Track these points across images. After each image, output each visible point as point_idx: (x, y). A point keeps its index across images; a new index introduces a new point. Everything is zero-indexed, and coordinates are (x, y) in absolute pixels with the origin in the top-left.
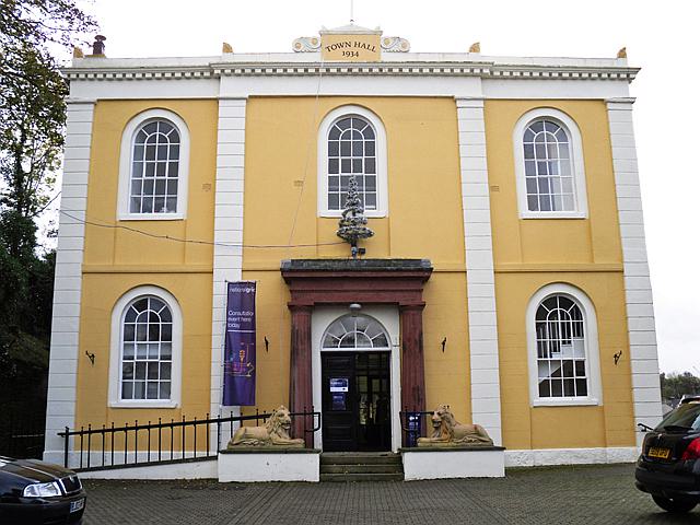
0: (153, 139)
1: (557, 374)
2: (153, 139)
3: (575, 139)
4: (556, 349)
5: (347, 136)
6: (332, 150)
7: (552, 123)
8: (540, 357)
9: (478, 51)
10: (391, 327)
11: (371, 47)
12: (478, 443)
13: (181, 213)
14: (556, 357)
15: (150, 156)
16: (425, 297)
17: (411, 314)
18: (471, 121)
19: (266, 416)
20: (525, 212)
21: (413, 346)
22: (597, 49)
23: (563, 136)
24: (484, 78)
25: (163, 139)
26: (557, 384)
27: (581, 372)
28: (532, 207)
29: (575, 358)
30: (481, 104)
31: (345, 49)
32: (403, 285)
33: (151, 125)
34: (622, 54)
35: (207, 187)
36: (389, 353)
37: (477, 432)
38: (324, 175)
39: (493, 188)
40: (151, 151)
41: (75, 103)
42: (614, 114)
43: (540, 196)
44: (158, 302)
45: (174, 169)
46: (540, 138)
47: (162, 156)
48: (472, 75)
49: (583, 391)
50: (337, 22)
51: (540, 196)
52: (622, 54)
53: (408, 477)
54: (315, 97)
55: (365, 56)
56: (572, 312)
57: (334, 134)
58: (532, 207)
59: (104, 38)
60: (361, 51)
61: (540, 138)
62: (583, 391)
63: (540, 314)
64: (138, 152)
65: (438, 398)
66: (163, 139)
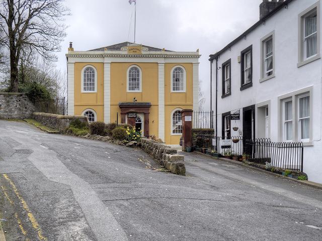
0: (88, 72)
1: (177, 128)
2: (133, 72)
3: (185, 73)
5: (88, 72)
7: (180, 69)
17: (146, 115)
18: (161, 69)
19: (320, 58)
20: (172, 91)
22: (192, 49)
23: (182, 72)
24: (165, 58)
28: (174, 90)
30: (164, 65)
32: (145, 108)
34: (198, 51)
35: (102, 85)
37: (160, 140)
39: (165, 85)
44: (91, 113)
45: (93, 81)
48: (162, 57)
52: (198, 51)
55: (138, 53)
58: (174, 90)
60: (137, 51)
63: (174, 115)
64: (85, 75)
65: (151, 134)
66: (90, 72)
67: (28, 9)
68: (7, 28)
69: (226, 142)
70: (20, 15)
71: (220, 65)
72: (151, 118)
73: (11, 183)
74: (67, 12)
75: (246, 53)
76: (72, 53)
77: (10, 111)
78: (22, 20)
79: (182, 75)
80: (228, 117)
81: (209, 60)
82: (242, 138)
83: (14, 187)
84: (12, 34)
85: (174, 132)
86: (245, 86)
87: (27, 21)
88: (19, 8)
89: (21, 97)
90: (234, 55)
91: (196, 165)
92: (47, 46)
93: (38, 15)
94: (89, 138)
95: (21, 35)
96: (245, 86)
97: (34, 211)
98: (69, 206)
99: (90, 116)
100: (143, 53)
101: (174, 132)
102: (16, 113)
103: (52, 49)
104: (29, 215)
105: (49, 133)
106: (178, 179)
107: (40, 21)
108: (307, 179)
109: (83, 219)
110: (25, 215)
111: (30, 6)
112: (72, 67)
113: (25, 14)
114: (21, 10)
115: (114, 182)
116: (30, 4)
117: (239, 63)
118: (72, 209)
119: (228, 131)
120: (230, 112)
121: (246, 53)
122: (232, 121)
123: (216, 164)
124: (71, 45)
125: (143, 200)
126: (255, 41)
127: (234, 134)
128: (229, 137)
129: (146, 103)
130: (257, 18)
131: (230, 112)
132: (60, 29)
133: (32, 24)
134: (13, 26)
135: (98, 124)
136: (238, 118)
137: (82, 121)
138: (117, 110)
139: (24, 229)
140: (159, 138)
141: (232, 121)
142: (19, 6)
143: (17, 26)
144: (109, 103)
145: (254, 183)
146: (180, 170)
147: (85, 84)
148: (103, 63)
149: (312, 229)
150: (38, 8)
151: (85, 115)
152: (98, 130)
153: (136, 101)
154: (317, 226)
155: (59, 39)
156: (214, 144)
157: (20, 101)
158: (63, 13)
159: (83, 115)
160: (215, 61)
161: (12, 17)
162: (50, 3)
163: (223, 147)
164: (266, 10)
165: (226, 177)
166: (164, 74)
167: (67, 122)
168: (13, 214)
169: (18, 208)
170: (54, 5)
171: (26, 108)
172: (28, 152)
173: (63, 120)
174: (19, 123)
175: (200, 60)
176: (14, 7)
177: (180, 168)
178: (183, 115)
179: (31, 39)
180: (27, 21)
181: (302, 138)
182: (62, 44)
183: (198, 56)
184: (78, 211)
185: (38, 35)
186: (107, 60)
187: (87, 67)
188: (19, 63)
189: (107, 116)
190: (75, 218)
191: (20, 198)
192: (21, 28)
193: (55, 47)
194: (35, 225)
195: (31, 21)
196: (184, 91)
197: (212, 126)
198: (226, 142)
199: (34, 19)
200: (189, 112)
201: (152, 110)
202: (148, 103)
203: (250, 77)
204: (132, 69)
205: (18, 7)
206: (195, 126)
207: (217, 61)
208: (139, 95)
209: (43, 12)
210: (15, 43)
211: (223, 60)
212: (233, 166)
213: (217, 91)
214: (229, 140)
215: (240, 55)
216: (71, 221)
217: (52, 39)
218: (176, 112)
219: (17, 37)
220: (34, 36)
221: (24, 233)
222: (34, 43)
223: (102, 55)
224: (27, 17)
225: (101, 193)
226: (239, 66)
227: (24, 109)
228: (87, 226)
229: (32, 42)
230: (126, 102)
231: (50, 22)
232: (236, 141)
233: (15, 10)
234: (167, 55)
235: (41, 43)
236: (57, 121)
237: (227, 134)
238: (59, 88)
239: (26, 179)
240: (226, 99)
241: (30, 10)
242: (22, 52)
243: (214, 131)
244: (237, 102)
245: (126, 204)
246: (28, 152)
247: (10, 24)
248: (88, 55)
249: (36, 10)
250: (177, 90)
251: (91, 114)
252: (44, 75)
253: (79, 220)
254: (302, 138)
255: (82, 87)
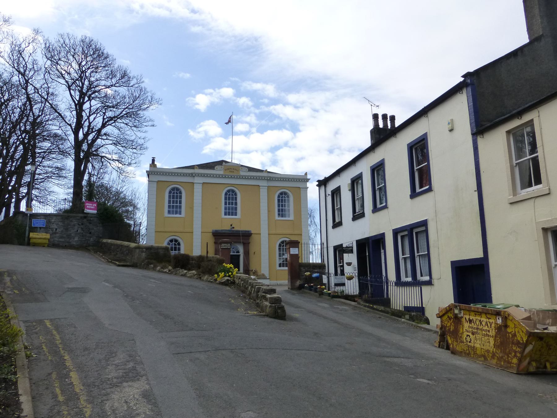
1: (284, 261)
2: (174, 193)
4: (283, 255)
6: (226, 199)
7: (285, 193)
9: (506, 132)
10: (241, 249)
12: (263, 277)
13: (183, 215)
14: (283, 257)
15: (173, 198)
16: (250, 241)
17: (246, 245)
18: (264, 193)
21: (247, 253)
23: (288, 197)
24: (267, 180)
25: (177, 193)
26: (283, 264)
32: (245, 237)
33: (173, 189)
35: (191, 208)
36: (239, 256)
37: (263, 275)
39: (268, 211)
42: (302, 190)
43: (282, 213)
44: (176, 241)
46: (282, 197)
47: (177, 198)
48: (265, 179)
49: (236, 215)
50: (262, 135)
51: (282, 213)
55: (235, 174)
57: (226, 194)
60: (235, 171)
61: (282, 197)
62: (236, 215)
63: (280, 245)
64: (170, 197)
65: (253, 267)
66: (177, 193)
67: (102, 117)
68: (72, 138)
69: (340, 279)
70: (90, 123)
71: (329, 192)
72: (253, 248)
73: (55, 332)
74: (150, 123)
75: (356, 181)
76: (154, 169)
77: (69, 236)
78: (92, 129)
79: (288, 200)
80: (340, 250)
81: (317, 185)
82: (357, 275)
83: (58, 337)
84: (78, 144)
85: (280, 266)
86: (357, 216)
87: (99, 131)
88: (90, 115)
89: (85, 220)
90: (344, 182)
91: (298, 305)
92: (123, 160)
93: (113, 125)
94: (170, 272)
95: (90, 146)
96: (357, 216)
97: (80, 368)
98: (127, 362)
99: (175, 245)
100: (242, 173)
101: (280, 266)
102: (75, 240)
103: (129, 164)
104: (72, 374)
105: (119, 266)
106: (277, 322)
107: (116, 132)
108: (429, 323)
109: (144, 378)
110: (67, 376)
111: (104, 113)
112: (155, 185)
113: (98, 122)
114: (92, 118)
115: (192, 329)
116: (104, 111)
117: (349, 190)
118: (131, 365)
119: (341, 266)
120: (342, 245)
121: (356, 181)
122: (345, 255)
123: (326, 305)
124: (153, 161)
125: (224, 352)
126: (364, 168)
127: (348, 270)
128: (343, 273)
129: (246, 231)
130: (367, 143)
131: (342, 245)
132: (141, 141)
133: (105, 134)
134: (81, 136)
135: (183, 255)
136: (351, 251)
137: (161, 252)
138: (211, 240)
139: (62, 393)
140: (262, 272)
141: (345, 255)
142: (90, 113)
143: (86, 135)
144: (200, 230)
145: (368, 328)
146: (278, 313)
147: (169, 207)
148: (193, 183)
149: (424, 383)
150: (114, 117)
151: (169, 244)
152: (183, 263)
153: (233, 228)
154: (429, 380)
155: (139, 152)
156: (325, 280)
157: (82, 224)
158: (145, 124)
159: (165, 244)
160: (323, 188)
161: (79, 125)
162: (129, 112)
163: (336, 285)
164: (377, 136)
165: (335, 322)
166: (267, 198)
167: (142, 252)
168: (50, 374)
169: (60, 365)
170: (134, 115)
171: (90, 233)
172: (83, 291)
173: (137, 251)
174: (80, 253)
175: (308, 184)
176: (84, 114)
177: (279, 311)
178: (288, 247)
179: (103, 152)
180: (99, 131)
181: (422, 276)
182: (142, 158)
183: (308, 180)
184: (139, 368)
185: (112, 148)
186: (197, 180)
187: (170, 187)
188: (86, 177)
189: (197, 246)
190: (131, 375)
191: (62, 352)
192: (90, 137)
193: (133, 162)
194: (78, 388)
195: (104, 131)
196: (292, 218)
197: (323, 259)
198: (340, 279)
199: (108, 129)
200: (295, 244)
201: (254, 238)
202: (248, 231)
203: (363, 206)
204: (229, 191)
205: (88, 114)
206: (306, 259)
207: (325, 187)
208: (239, 222)
209: (120, 121)
210: (82, 154)
211: (332, 186)
212: (347, 307)
213: (326, 220)
214: (342, 277)
215: (350, 182)
216: (127, 382)
217: (128, 152)
218: (283, 242)
219: (85, 147)
220: (107, 148)
221: (61, 398)
222: (107, 155)
223: (192, 174)
224: (99, 125)
225: (172, 343)
226: (350, 194)
227: (88, 235)
228: (147, 387)
229: (103, 155)
230: (221, 229)
231: (128, 132)
232: (350, 278)
233: (85, 117)
234: (271, 177)
235: (115, 157)
236: (130, 251)
237: (340, 271)
238: (137, 209)
239: (75, 327)
240: (377, 214)
241: (104, 119)
242: (90, 166)
243: (325, 266)
244: (351, 233)
245: (202, 357)
246: (83, 291)
247: (76, 133)
248: (175, 173)
249: (111, 119)
250: (282, 217)
251: (175, 243)
252: (118, 193)
253: (138, 380)
254: (422, 276)
255: (166, 209)
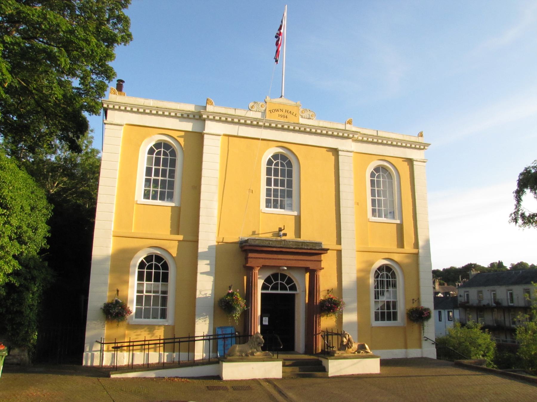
1: (382, 308)
2: (159, 153)
8: (376, 299)
11: (294, 114)
27: (395, 307)
29: (392, 300)
31: (281, 113)
38: (264, 187)
40: (276, 171)
41: (111, 124)
49: (395, 319)
53: (330, 375)
54: (258, 139)
56: (392, 275)
59: (123, 82)
60: (289, 115)
61: (378, 177)
62: (395, 319)
